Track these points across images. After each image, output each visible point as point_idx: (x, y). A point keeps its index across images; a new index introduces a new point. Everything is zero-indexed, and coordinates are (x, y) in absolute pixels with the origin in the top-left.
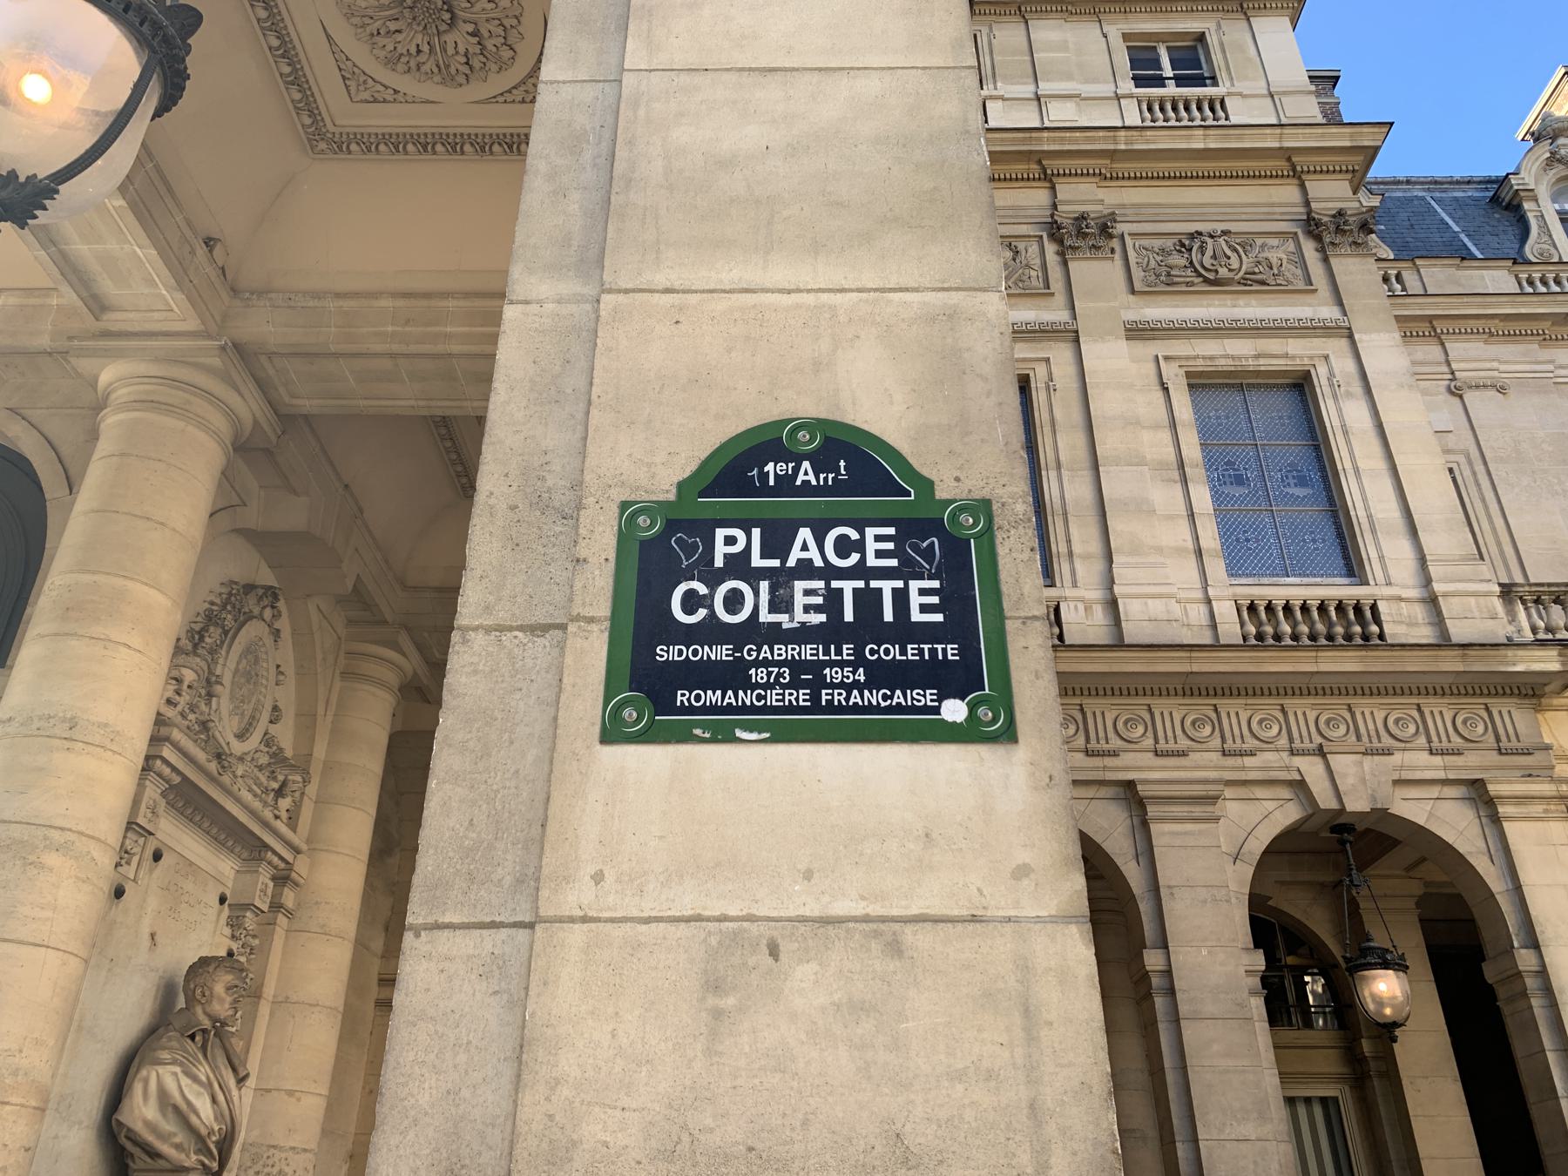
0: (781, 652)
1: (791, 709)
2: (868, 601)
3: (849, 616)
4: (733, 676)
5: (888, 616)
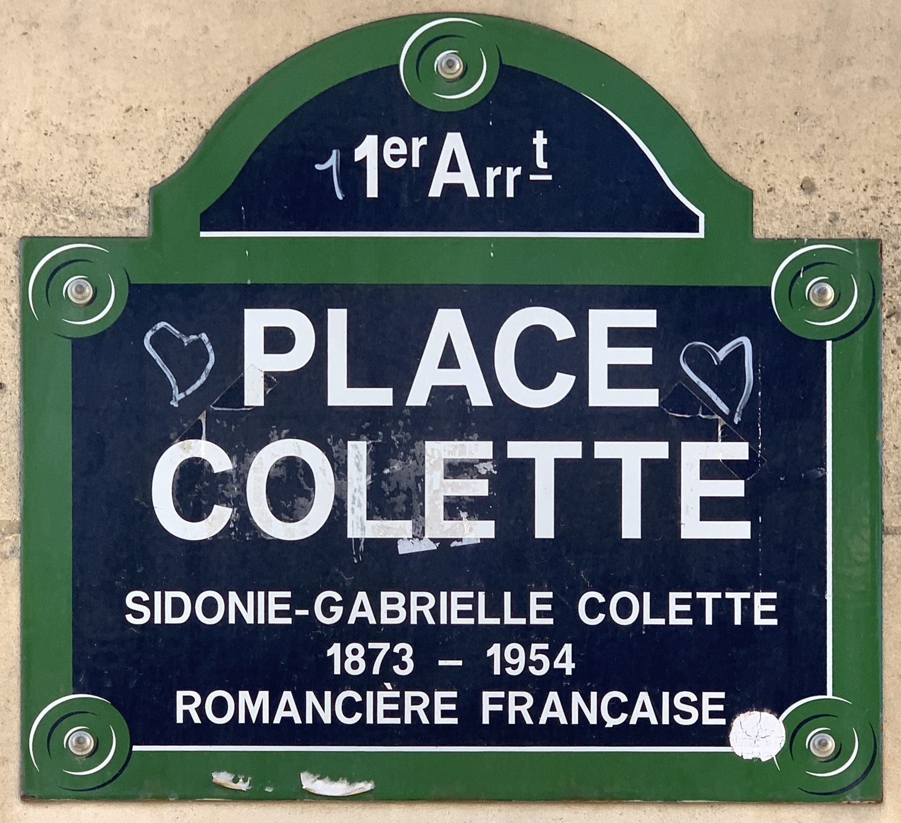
0: (397, 607)
2: (591, 487)
4: (293, 660)
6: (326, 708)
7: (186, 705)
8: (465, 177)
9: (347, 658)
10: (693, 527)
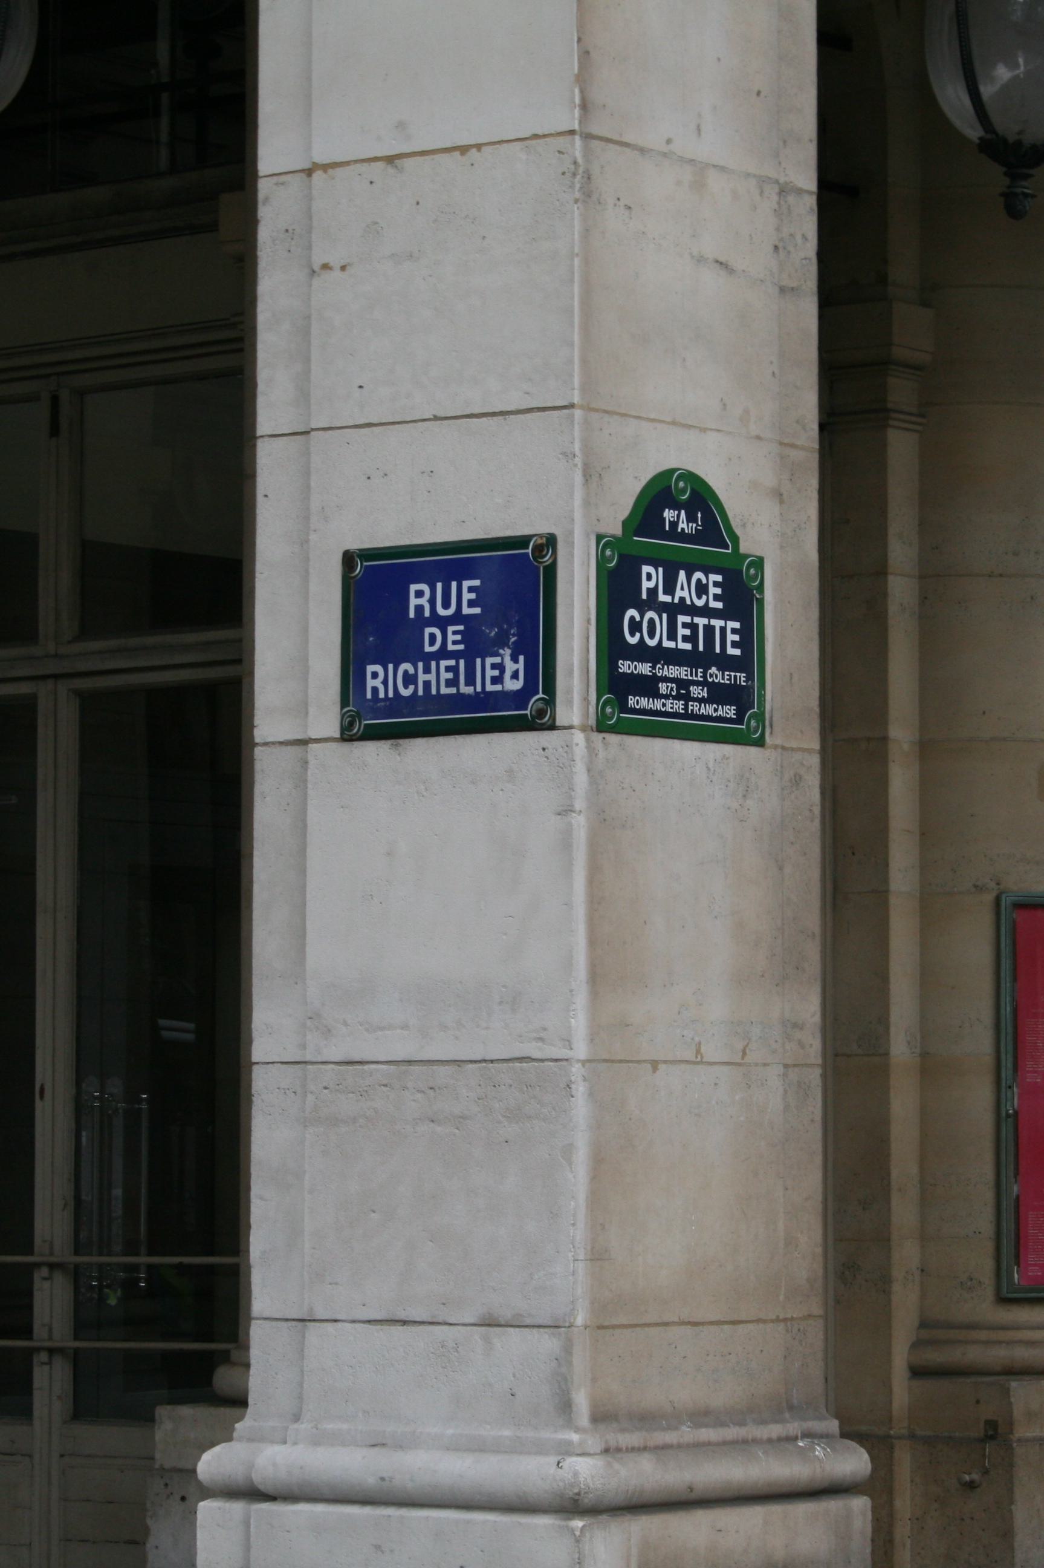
0: (673, 671)
1: (720, 719)
3: (701, 648)
5: (718, 650)
6: (657, 705)
7: (632, 701)
8: (685, 526)
9: (663, 688)
10: (451, 647)
